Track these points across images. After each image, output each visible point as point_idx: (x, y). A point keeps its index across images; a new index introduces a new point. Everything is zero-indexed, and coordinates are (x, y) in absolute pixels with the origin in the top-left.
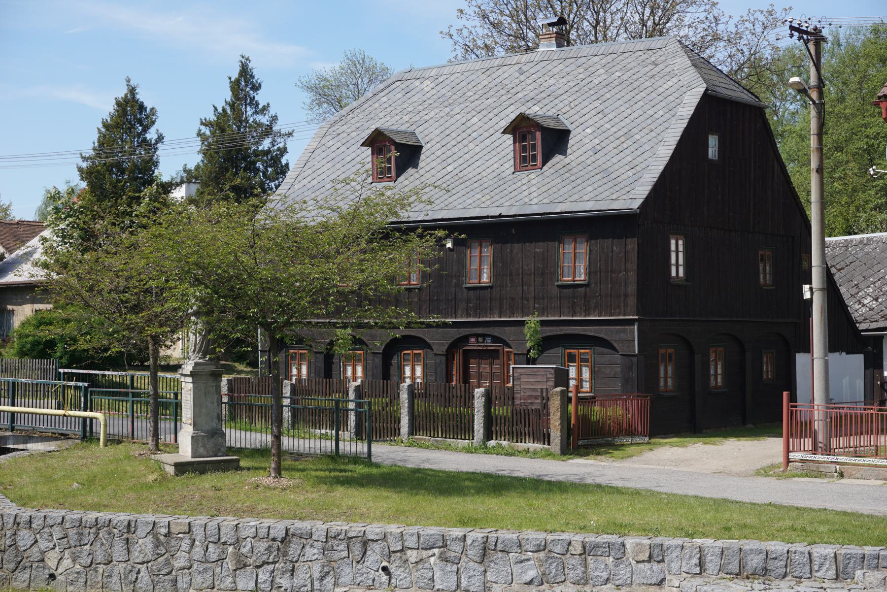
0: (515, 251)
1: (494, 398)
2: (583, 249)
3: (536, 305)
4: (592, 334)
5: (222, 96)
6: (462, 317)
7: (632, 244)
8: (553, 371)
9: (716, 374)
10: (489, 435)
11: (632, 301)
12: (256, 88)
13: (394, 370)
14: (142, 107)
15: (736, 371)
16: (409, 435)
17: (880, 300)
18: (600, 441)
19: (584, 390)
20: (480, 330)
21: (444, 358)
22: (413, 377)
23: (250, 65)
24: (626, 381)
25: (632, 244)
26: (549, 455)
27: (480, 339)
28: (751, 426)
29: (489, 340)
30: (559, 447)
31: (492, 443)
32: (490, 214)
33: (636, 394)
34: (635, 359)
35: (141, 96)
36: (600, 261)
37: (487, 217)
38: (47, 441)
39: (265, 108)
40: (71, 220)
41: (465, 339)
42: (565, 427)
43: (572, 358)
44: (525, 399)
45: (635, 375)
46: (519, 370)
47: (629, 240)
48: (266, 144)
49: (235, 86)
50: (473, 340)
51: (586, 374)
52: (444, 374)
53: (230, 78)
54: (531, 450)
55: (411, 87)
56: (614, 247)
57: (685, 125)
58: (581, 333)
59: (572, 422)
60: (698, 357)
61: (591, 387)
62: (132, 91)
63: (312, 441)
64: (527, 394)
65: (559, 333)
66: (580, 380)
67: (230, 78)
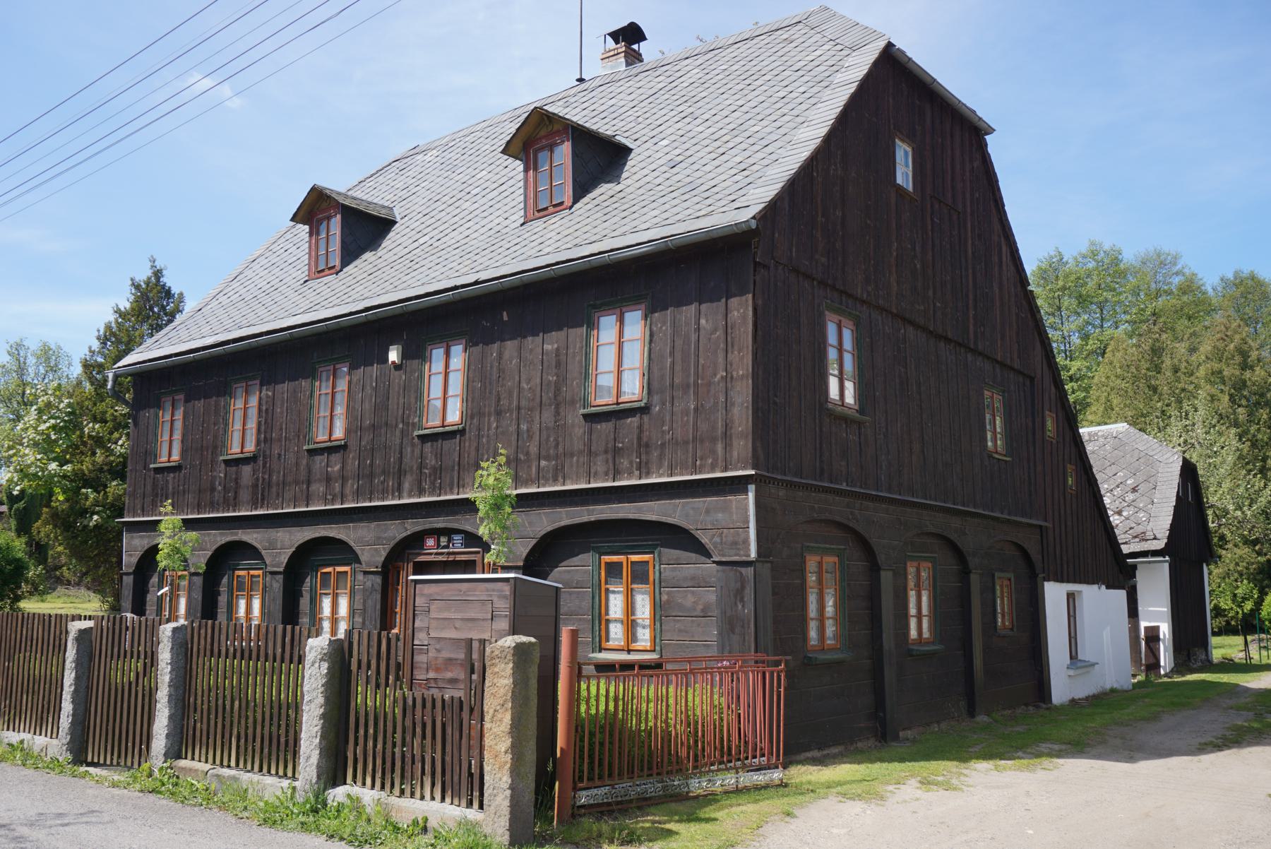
0: (507, 355)
1: (354, 667)
2: (635, 325)
4: (654, 518)
6: (410, 496)
7: (741, 309)
8: (507, 589)
9: (919, 616)
10: (334, 773)
11: (742, 446)
13: (304, 602)
14: (168, 294)
15: (955, 609)
16: (167, 756)
17: (1125, 514)
18: (652, 787)
19: (611, 644)
20: (439, 522)
21: (378, 580)
24: (730, 625)
25: (741, 309)
27: (444, 540)
28: (986, 719)
29: (458, 539)
30: (504, 822)
31: (338, 794)
32: (458, 284)
33: (752, 655)
34: (749, 572)
35: (168, 280)
36: (672, 353)
37: (456, 288)
40: (53, 421)
41: (415, 541)
42: (531, 756)
43: (614, 571)
44: (437, 670)
45: (748, 610)
46: (427, 589)
47: (734, 302)
50: (430, 542)
51: (644, 609)
52: (378, 613)
56: (702, 319)
57: (852, 90)
58: (631, 516)
59: (561, 742)
60: (886, 577)
61: (654, 640)
62: (158, 274)
64: (446, 654)
65: (585, 519)
66: (631, 626)
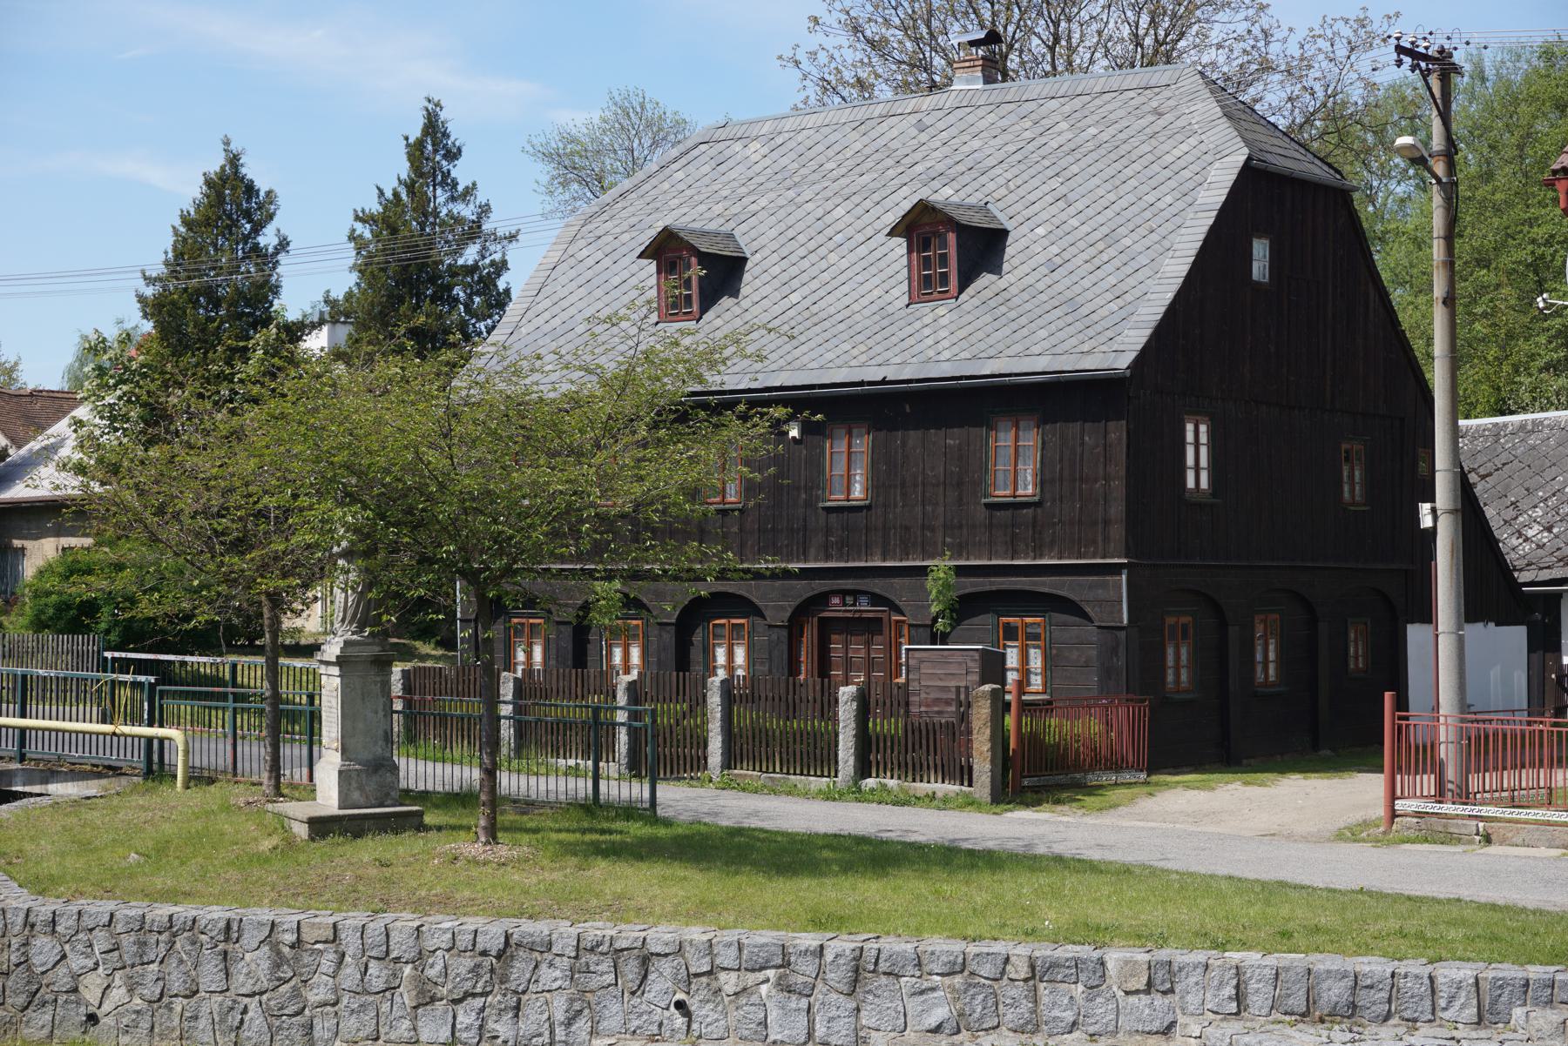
0: (910, 443)
1: (873, 704)
2: (1031, 439)
3: (948, 540)
4: (1046, 590)
5: (392, 170)
6: (816, 560)
7: (1117, 432)
8: (977, 656)
9: (1266, 662)
10: (864, 769)
11: (1118, 532)
12: (453, 155)
13: (696, 654)
14: (250, 190)
15: (1301, 656)
16: (723, 768)
17: (1555, 530)
18: (1061, 779)
19: (1032, 688)
20: (848, 584)
21: (785, 633)
22: (730, 666)
23: (443, 115)
24: (1107, 673)
25: (1117, 432)
26: (970, 803)
27: (849, 600)
28: (1328, 752)
29: (864, 600)
30: (987, 790)
31: (870, 782)
32: (867, 379)
33: (1124, 696)
34: (1122, 634)
35: (250, 170)
36: (1061, 460)
37: (862, 383)
38: (83, 779)
39: (469, 191)
40: (125, 388)
41: (822, 599)
42: (1000, 755)
43: (1011, 633)
44: (927, 706)
45: (1122, 662)
46: (917, 654)
47: (1112, 425)
48: (470, 254)
49: (416, 152)
50: (836, 600)
51: (1036, 660)
52: (785, 662)
53: (407, 139)
54: (939, 795)
55: (727, 153)
56: (1085, 436)
57: (1211, 222)
58: (1027, 588)
59: (1012, 746)
60: (1233, 632)
61: (1045, 684)
62: (234, 160)
63: (552, 779)
64: (932, 696)
65: (987, 588)
66: (1025, 672)
67: (407, 139)
